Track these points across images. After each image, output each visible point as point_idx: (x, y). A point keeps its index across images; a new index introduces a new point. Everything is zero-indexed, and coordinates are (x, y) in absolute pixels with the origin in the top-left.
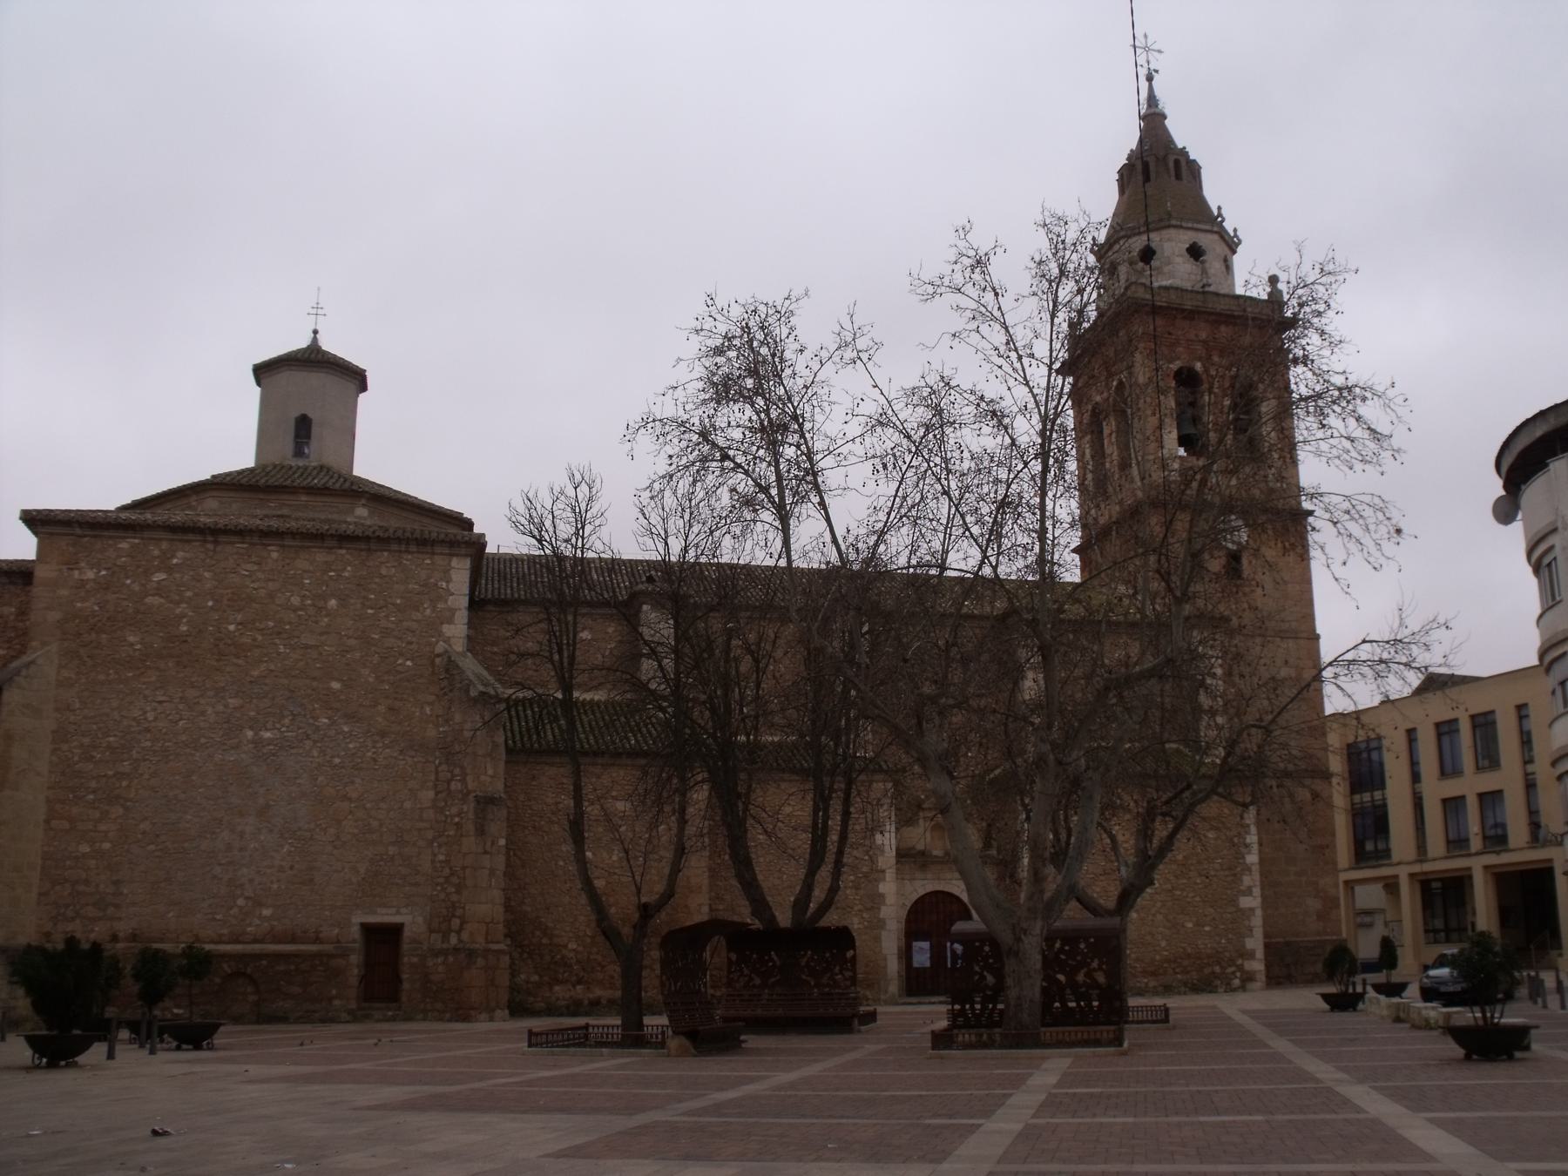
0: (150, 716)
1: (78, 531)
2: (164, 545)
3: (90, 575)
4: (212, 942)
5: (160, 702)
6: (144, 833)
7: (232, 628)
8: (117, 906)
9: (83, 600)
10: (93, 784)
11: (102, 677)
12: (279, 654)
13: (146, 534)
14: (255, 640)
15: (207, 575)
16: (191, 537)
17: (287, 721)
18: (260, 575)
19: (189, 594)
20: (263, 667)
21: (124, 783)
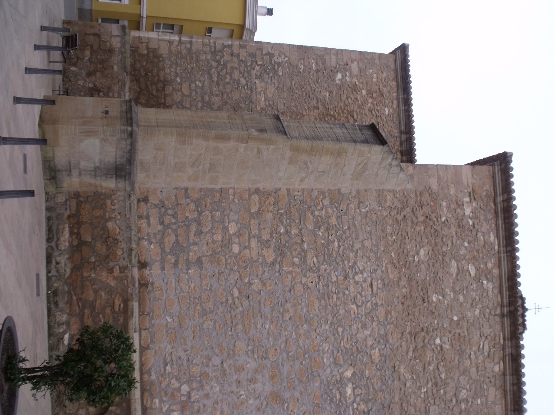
0: (359, 278)
1: (500, 199)
2: (496, 271)
3: (468, 211)
4: (142, 365)
5: (371, 285)
6: (250, 284)
7: (438, 341)
8: (176, 264)
9: (448, 207)
10: (294, 231)
11: (389, 230)
12: (419, 388)
13: (503, 255)
14: (429, 364)
15: (477, 312)
16: (506, 293)
17: (362, 407)
18: (481, 358)
19: (461, 298)
20: (408, 376)
21: (296, 260)
